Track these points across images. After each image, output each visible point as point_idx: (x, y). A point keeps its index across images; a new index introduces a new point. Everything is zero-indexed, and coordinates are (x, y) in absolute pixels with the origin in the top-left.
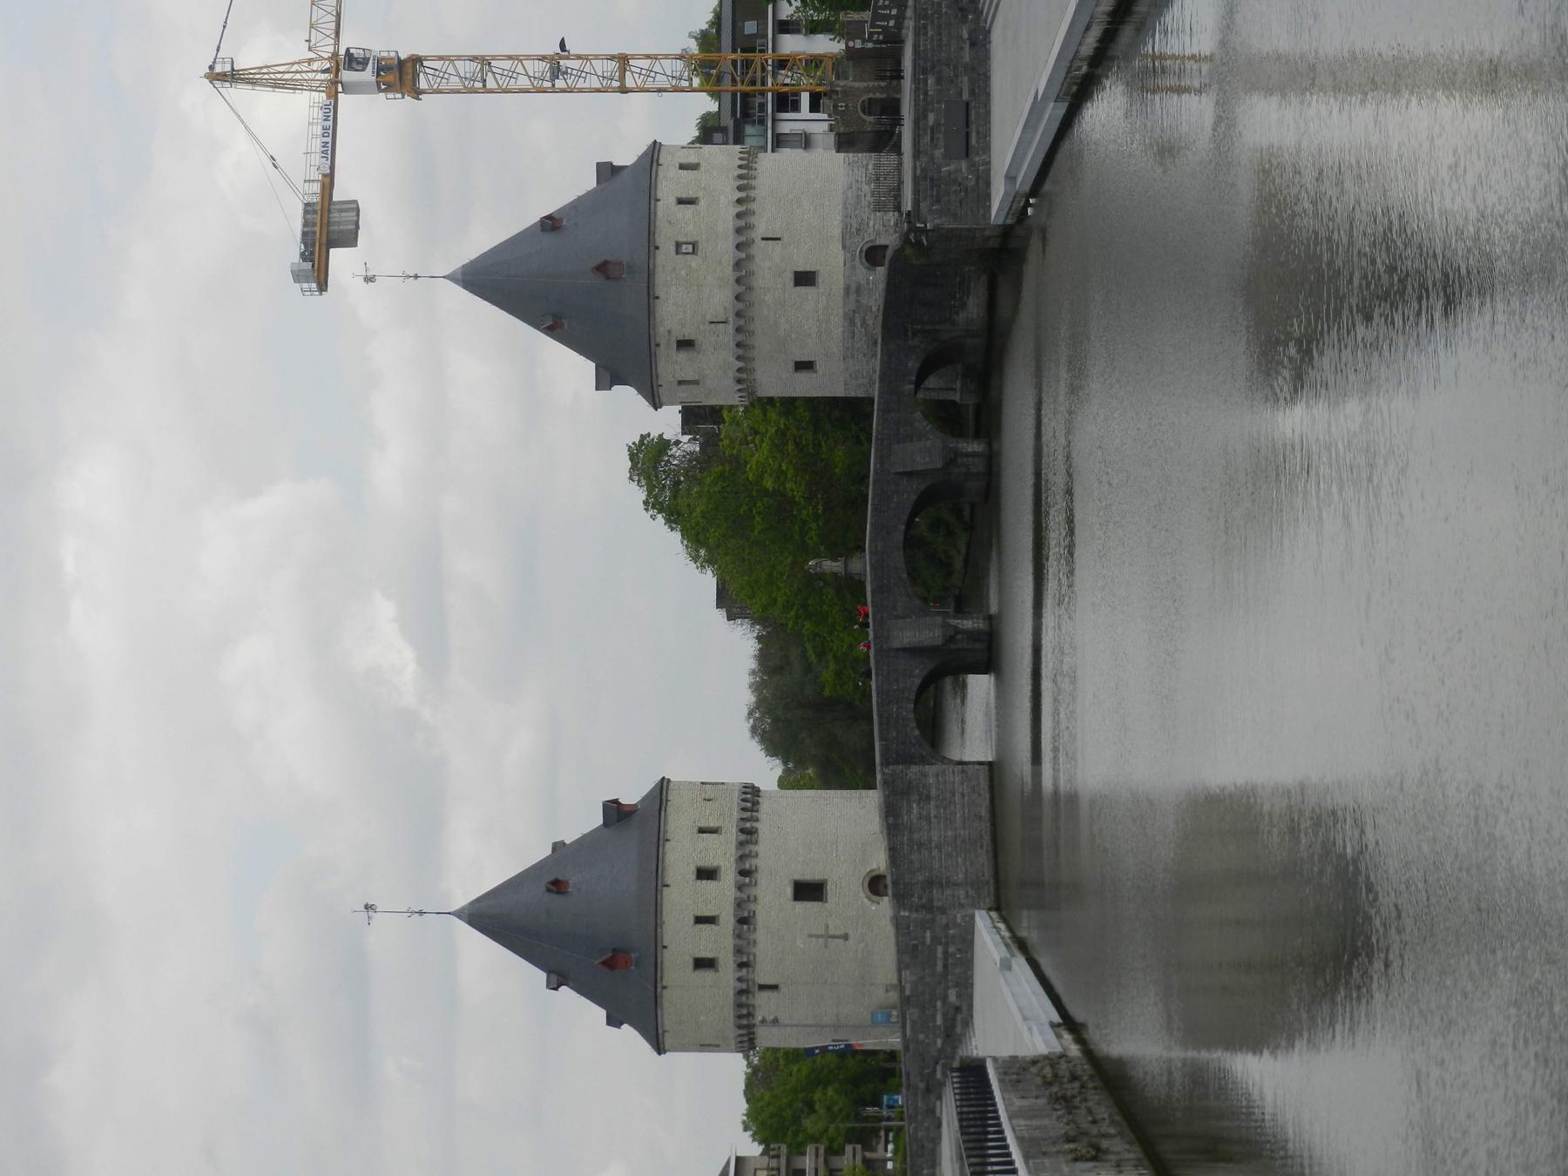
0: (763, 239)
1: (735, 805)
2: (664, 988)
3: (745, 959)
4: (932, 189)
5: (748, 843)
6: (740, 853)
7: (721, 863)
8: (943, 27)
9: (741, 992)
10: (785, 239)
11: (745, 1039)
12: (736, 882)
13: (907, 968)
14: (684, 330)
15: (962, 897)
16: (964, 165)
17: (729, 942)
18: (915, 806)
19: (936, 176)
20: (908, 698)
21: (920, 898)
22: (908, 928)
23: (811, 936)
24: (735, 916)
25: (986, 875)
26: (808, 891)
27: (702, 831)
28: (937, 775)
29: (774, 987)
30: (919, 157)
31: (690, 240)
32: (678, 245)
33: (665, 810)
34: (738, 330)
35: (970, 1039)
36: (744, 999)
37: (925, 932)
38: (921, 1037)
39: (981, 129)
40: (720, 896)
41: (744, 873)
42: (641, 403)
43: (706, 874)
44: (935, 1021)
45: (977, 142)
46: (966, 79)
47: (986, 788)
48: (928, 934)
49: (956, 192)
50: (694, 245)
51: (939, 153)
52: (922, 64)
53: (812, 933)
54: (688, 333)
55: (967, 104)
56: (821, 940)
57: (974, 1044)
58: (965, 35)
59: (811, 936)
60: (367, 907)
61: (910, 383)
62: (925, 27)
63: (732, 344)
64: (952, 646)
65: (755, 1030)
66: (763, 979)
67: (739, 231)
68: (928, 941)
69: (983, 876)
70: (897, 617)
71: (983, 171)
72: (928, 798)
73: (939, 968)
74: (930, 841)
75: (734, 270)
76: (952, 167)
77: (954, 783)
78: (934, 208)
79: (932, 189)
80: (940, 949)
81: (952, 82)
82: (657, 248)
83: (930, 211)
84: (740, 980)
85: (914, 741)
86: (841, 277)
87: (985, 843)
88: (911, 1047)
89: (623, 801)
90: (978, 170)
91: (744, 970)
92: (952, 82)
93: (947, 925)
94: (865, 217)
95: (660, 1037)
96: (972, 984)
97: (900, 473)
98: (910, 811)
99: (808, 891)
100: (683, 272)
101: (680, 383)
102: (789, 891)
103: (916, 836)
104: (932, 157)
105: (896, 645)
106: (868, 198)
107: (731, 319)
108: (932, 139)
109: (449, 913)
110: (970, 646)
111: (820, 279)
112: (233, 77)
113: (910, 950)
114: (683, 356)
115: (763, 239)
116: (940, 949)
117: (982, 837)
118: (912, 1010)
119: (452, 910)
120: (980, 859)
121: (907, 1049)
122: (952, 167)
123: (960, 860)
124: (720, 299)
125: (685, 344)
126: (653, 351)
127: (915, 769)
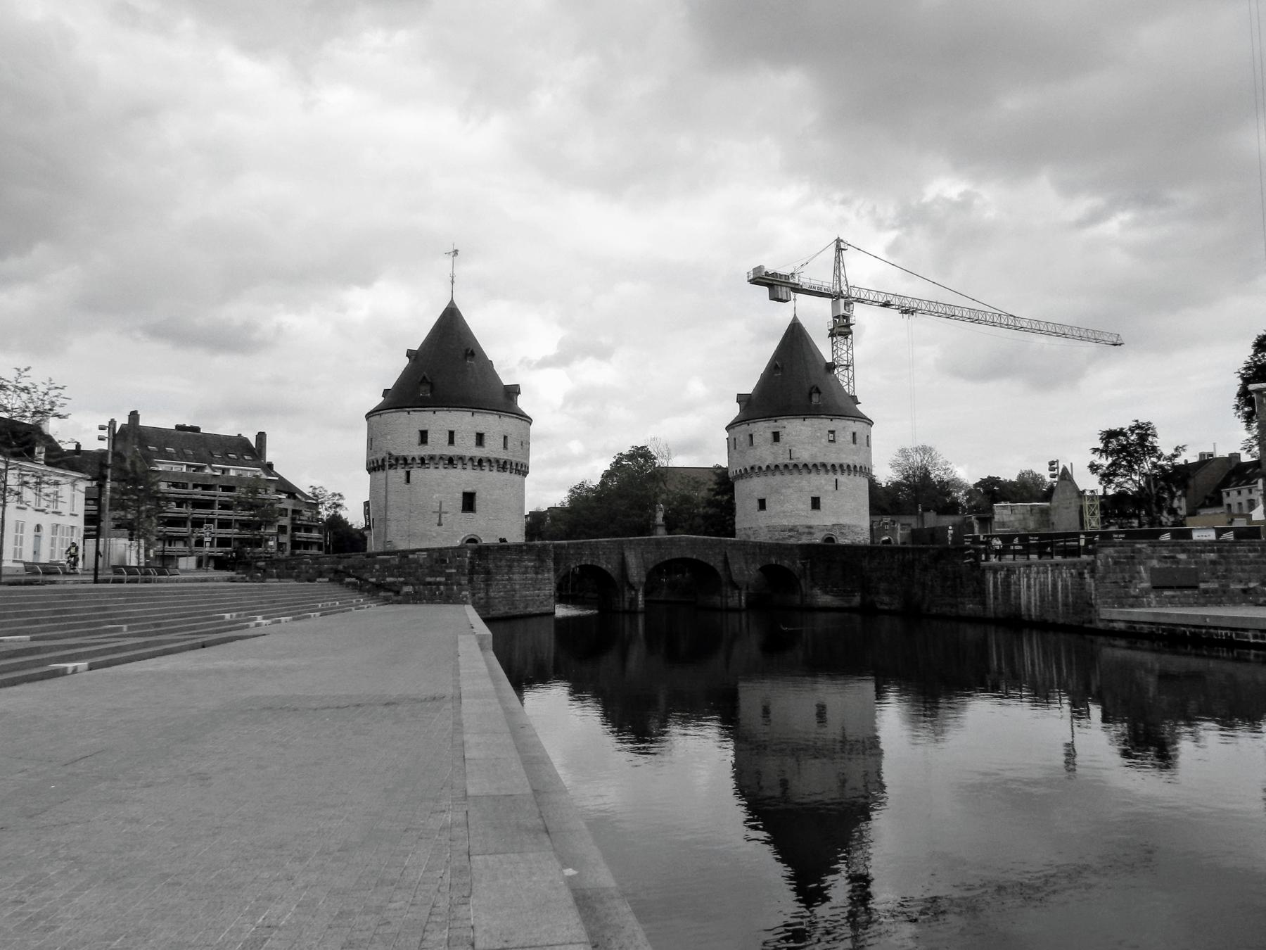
0: (836, 480)
1: (519, 460)
2: (409, 413)
3: (426, 462)
4: (1126, 557)
5: (498, 465)
6: (492, 460)
7: (486, 449)
8: (1257, 566)
9: (405, 459)
10: (836, 492)
11: (375, 465)
12: (475, 457)
13: (429, 555)
14: (785, 435)
15: (479, 595)
16: (1146, 585)
17: (437, 452)
18: (532, 564)
19: (1136, 561)
20: (593, 561)
21: (479, 565)
22: (458, 557)
23: (441, 503)
24: (454, 456)
25: (494, 612)
26: (469, 502)
27: (505, 438)
28: (549, 579)
29: (408, 481)
30: (1150, 546)
31: (836, 438)
32: (832, 432)
33: (517, 418)
34: (786, 466)
35: (374, 603)
36: (401, 462)
37: (455, 568)
38: (377, 567)
39: (1177, 599)
40: (466, 447)
41: (480, 461)
43: (480, 439)
44: (389, 576)
45: (1166, 597)
46: (1216, 586)
47: (542, 611)
48: (454, 571)
49: (1124, 578)
50: (833, 441)
51: (1155, 563)
52: (1225, 548)
53: (443, 504)
54: (783, 438)
55: (1196, 588)
56: (438, 509)
57: (372, 605)
58: (1252, 585)
59: (441, 503)
60: (456, 252)
61: (776, 561)
62: (1256, 551)
63: (777, 463)
64: (626, 588)
65: (381, 471)
66: (413, 472)
67: (841, 466)
68: (448, 571)
69: (493, 610)
70: (642, 554)
71: (1143, 601)
72: (537, 573)
73: (428, 579)
74: (513, 574)
75: (821, 463)
76: (1144, 575)
77: (545, 590)
78: (1110, 560)
79: (1126, 557)
80: (443, 579)
81: (1213, 574)
82: (831, 420)
83: (1107, 557)
84: (413, 459)
85: (567, 565)
86: (818, 524)
87: (512, 611)
88: (369, 559)
89: (519, 397)
90: (1143, 597)
91: (419, 461)
92: (1213, 574)
93: (460, 584)
94: (849, 538)
95: (377, 413)
96: (416, 603)
97: (726, 555)
98: (530, 560)
99: (469, 502)
100: (819, 434)
101: (751, 436)
102: (469, 490)
103: (516, 564)
104: (1152, 558)
105: (627, 553)
106: (858, 539)
107: (792, 461)
108: (1165, 557)
110: (626, 599)
111: (815, 511)
112: (839, 249)
113: (440, 558)
114: (769, 436)
115: (836, 480)
116: (443, 579)
117: (516, 608)
118: (397, 560)
119: (454, 299)
120: (502, 608)
121: (369, 556)
122: (1144, 575)
123: (502, 593)
124: (804, 455)
125: (776, 437)
127: (552, 565)
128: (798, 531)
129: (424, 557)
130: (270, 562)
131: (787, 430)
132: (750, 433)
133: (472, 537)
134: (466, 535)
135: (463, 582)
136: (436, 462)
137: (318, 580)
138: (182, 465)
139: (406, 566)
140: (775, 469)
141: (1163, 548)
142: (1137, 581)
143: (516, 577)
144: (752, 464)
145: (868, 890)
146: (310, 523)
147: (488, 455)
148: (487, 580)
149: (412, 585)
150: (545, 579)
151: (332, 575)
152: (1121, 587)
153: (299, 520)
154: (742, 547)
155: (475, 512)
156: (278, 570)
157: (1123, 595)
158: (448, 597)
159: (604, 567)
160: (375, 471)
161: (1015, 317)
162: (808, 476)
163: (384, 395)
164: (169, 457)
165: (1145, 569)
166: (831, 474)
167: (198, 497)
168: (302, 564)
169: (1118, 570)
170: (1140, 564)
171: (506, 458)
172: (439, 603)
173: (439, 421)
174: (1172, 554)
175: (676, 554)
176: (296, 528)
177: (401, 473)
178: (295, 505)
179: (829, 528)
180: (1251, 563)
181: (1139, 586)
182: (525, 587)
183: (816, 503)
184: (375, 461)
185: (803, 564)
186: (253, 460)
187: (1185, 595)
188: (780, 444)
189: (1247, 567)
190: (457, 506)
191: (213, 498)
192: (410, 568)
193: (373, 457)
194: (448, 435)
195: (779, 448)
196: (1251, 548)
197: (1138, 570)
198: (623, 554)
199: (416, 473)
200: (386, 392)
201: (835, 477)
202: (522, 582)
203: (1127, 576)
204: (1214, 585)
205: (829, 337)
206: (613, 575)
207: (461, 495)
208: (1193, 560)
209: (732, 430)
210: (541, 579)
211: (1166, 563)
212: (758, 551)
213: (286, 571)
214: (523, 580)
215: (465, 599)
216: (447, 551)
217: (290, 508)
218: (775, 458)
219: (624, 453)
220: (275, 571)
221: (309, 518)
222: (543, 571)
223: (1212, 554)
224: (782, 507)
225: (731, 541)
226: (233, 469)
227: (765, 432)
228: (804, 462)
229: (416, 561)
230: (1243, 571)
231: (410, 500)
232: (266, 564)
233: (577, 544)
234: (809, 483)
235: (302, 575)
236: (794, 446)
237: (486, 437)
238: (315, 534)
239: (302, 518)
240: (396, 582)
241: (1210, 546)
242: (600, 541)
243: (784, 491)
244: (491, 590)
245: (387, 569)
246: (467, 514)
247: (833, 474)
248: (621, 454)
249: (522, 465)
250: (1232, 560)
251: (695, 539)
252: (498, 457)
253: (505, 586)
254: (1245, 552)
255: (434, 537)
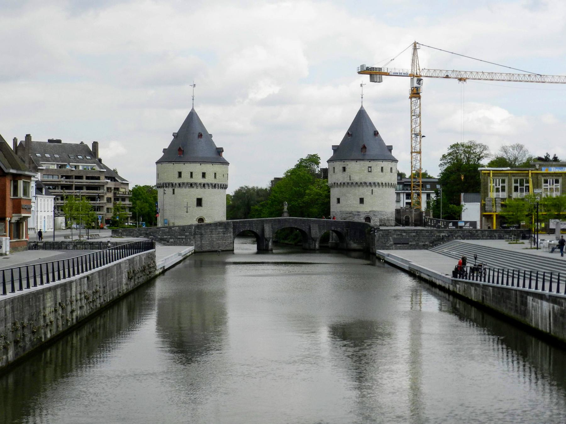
1: (222, 183)
2: (174, 164)
4: (386, 234)
6: (209, 184)
9: (172, 184)
16: (392, 243)
17: (186, 181)
19: (389, 235)
21: (198, 232)
23: (187, 203)
26: (199, 202)
27: (215, 174)
29: (174, 193)
34: (348, 183)
36: (171, 185)
38: (161, 232)
40: (198, 179)
41: (204, 185)
43: (204, 175)
45: (398, 246)
46: (415, 243)
48: (188, 234)
49: (385, 241)
50: (371, 171)
51: (395, 236)
54: (347, 170)
55: (408, 244)
56: (186, 205)
58: (426, 243)
59: (187, 203)
60: (195, 85)
62: (429, 232)
66: (176, 190)
67: (374, 183)
72: (224, 234)
73: (179, 237)
76: (391, 240)
79: (386, 234)
80: (184, 237)
83: (380, 234)
91: (178, 185)
98: (220, 229)
99: (199, 202)
101: (334, 168)
102: (199, 197)
105: (265, 225)
106: (383, 218)
107: (351, 181)
108: (399, 234)
111: (361, 205)
112: (415, 49)
113: (183, 229)
114: (341, 168)
121: (158, 228)
122: (391, 240)
124: (356, 178)
125: (344, 169)
127: (232, 230)
131: (349, 166)
133: (201, 217)
138: (54, 164)
147: (208, 182)
149: (173, 239)
151: (145, 235)
155: (202, 207)
161: (541, 75)
164: (47, 160)
167: (64, 183)
173: (186, 168)
175: (287, 225)
176: (116, 199)
178: (115, 185)
179: (368, 212)
183: (362, 201)
186: (91, 159)
188: (346, 173)
191: (71, 183)
192: (173, 233)
193: (159, 182)
199: (176, 190)
200: (165, 150)
201: (372, 188)
203: (386, 240)
210: (226, 236)
212: (326, 224)
217: (113, 187)
219: (304, 158)
221: (123, 193)
222: (227, 233)
226: (81, 165)
229: (175, 230)
230: (424, 239)
235: (135, 235)
243: (347, 195)
245: (164, 233)
246: (199, 208)
247: (370, 187)
248: (302, 159)
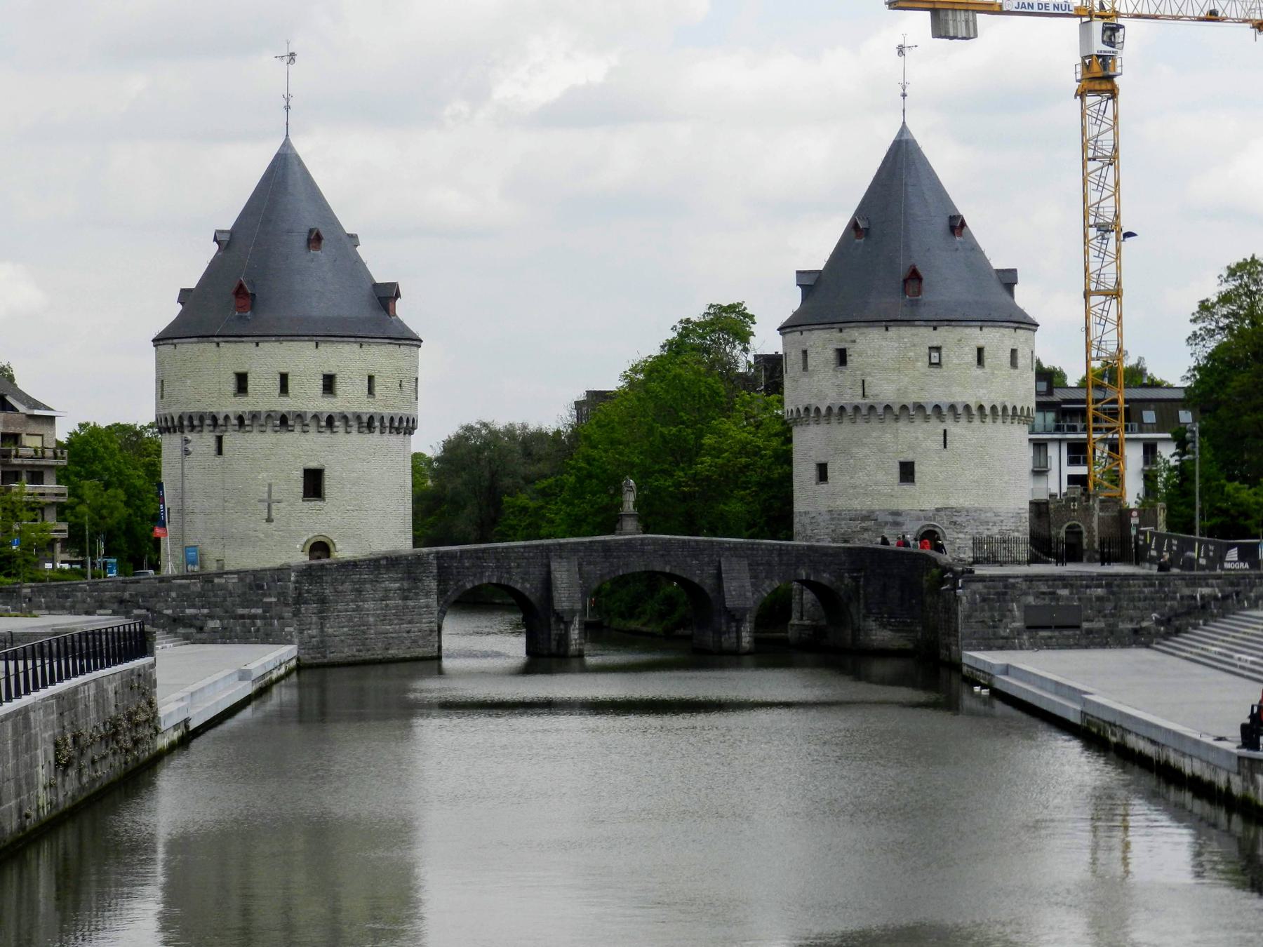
0: (945, 431)
2: (218, 344)
3: (247, 422)
6: (350, 416)
9: (214, 418)
10: (945, 452)
11: (169, 424)
12: (322, 413)
13: (241, 580)
16: (1017, 624)
18: (397, 585)
19: (1008, 597)
21: (308, 592)
23: (270, 485)
24: (289, 412)
26: (314, 483)
27: (371, 379)
28: (427, 606)
29: (220, 451)
30: (1026, 581)
31: (943, 360)
34: (857, 408)
36: (208, 422)
38: (174, 594)
40: (308, 399)
41: (330, 420)
42: (785, 315)
43: (329, 383)
44: (189, 607)
45: (1042, 638)
46: (1102, 625)
50: (939, 364)
51: (1031, 600)
54: (853, 359)
55: (1078, 627)
56: (266, 496)
59: (270, 485)
60: (292, 55)
61: (808, 575)
63: (843, 402)
64: (553, 620)
66: (226, 439)
67: (952, 407)
68: (266, 600)
71: (1014, 643)
72: (406, 598)
73: (240, 611)
75: (914, 404)
76: (1017, 613)
77: (421, 623)
79: (997, 594)
80: (260, 611)
83: (974, 593)
84: (227, 417)
88: (163, 584)
89: (398, 302)
90: (1014, 638)
91: (235, 422)
96: (225, 643)
99: (314, 483)
100: (912, 354)
101: (805, 352)
102: (313, 465)
104: (1026, 594)
105: (554, 565)
106: (986, 533)
107: (867, 401)
108: (1044, 593)
109: (287, 135)
110: (553, 637)
113: (256, 582)
114: (831, 355)
115: (945, 431)
116: (260, 611)
118: (199, 585)
122: (1017, 613)
124: (886, 390)
125: (842, 357)
126: (835, 326)
128: (876, 520)
129: (234, 581)
130: (35, 589)
132: (804, 348)
134: (310, 536)
135: (286, 615)
136: (260, 423)
137: (98, 612)
139: (211, 594)
140: (840, 413)
141: (1041, 583)
142: (1008, 620)
143: (369, 605)
144: (806, 402)
145: (159, 634)
146: (38, 462)
147: (343, 409)
148: (321, 612)
149: (220, 619)
150: (421, 607)
151: (115, 606)
152: (989, 627)
153: (16, 456)
154: (749, 552)
155: (324, 500)
156: (48, 600)
157: (992, 637)
158: (267, 635)
159: (518, 586)
160: (169, 432)
162: (894, 425)
163: (181, 300)
165: (1018, 607)
166: (934, 421)
168: (77, 591)
169: (986, 607)
170: (1012, 601)
171: (372, 410)
172: (256, 643)
174: (1051, 590)
177: (209, 438)
180: (1145, 599)
181: (1009, 626)
182: (384, 619)
184: (169, 418)
185: (854, 579)
187: (1064, 635)
188: (847, 371)
189: (1140, 604)
190: (296, 490)
192: (216, 596)
194: (278, 380)
195: (848, 376)
196: (1147, 582)
197: (1010, 607)
198: (548, 566)
201: (942, 426)
202: (378, 612)
204: (1099, 624)
205: (1076, 98)
206: (533, 598)
207: (300, 474)
208: (1076, 596)
209: (796, 335)
210: (414, 607)
211: (1044, 599)
213: (57, 600)
214: (382, 609)
215: (289, 637)
216: (264, 572)
218: (840, 394)
220: (43, 600)
221: (36, 451)
222: (417, 594)
223: (1099, 590)
224: (852, 478)
225: (729, 543)
227: (824, 348)
228: (887, 402)
230: (1135, 608)
231: (223, 482)
232: (32, 591)
233: (476, 551)
234: (896, 437)
235: (77, 606)
236: (870, 374)
237: (338, 380)
238: (50, 486)
239: (22, 451)
240: (197, 614)
241: (1097, 580)
242: (512, 548)
243: (855, 450)
244: (328, 625)
245: (187, 597)
249: (408, 419)
250: (1122, 596)
251: (670, 540)
252: (359, 411)
253: (350, 619)
254: (1139, 587)
255: (261, 540)
